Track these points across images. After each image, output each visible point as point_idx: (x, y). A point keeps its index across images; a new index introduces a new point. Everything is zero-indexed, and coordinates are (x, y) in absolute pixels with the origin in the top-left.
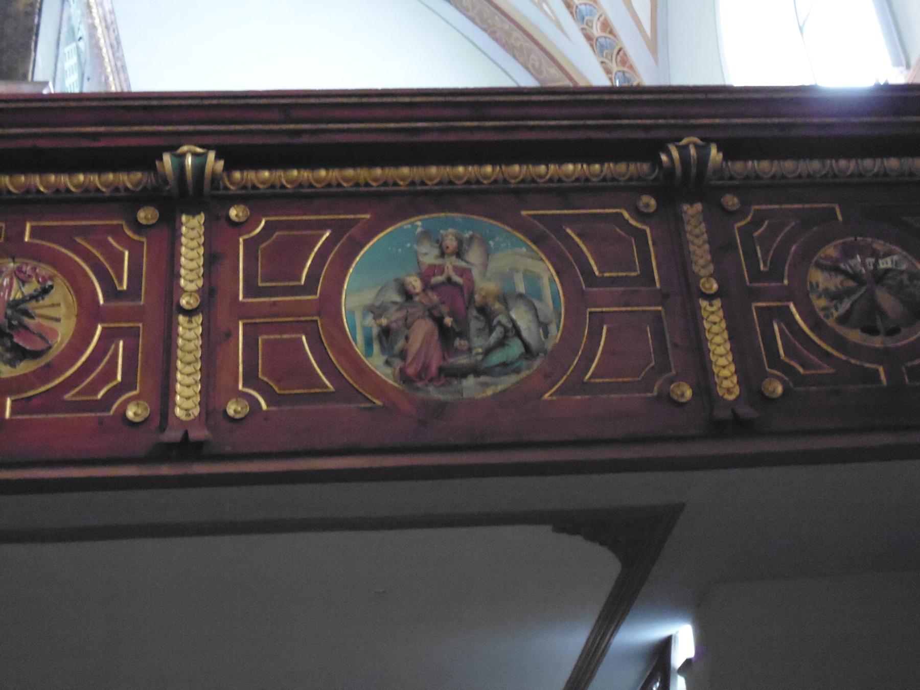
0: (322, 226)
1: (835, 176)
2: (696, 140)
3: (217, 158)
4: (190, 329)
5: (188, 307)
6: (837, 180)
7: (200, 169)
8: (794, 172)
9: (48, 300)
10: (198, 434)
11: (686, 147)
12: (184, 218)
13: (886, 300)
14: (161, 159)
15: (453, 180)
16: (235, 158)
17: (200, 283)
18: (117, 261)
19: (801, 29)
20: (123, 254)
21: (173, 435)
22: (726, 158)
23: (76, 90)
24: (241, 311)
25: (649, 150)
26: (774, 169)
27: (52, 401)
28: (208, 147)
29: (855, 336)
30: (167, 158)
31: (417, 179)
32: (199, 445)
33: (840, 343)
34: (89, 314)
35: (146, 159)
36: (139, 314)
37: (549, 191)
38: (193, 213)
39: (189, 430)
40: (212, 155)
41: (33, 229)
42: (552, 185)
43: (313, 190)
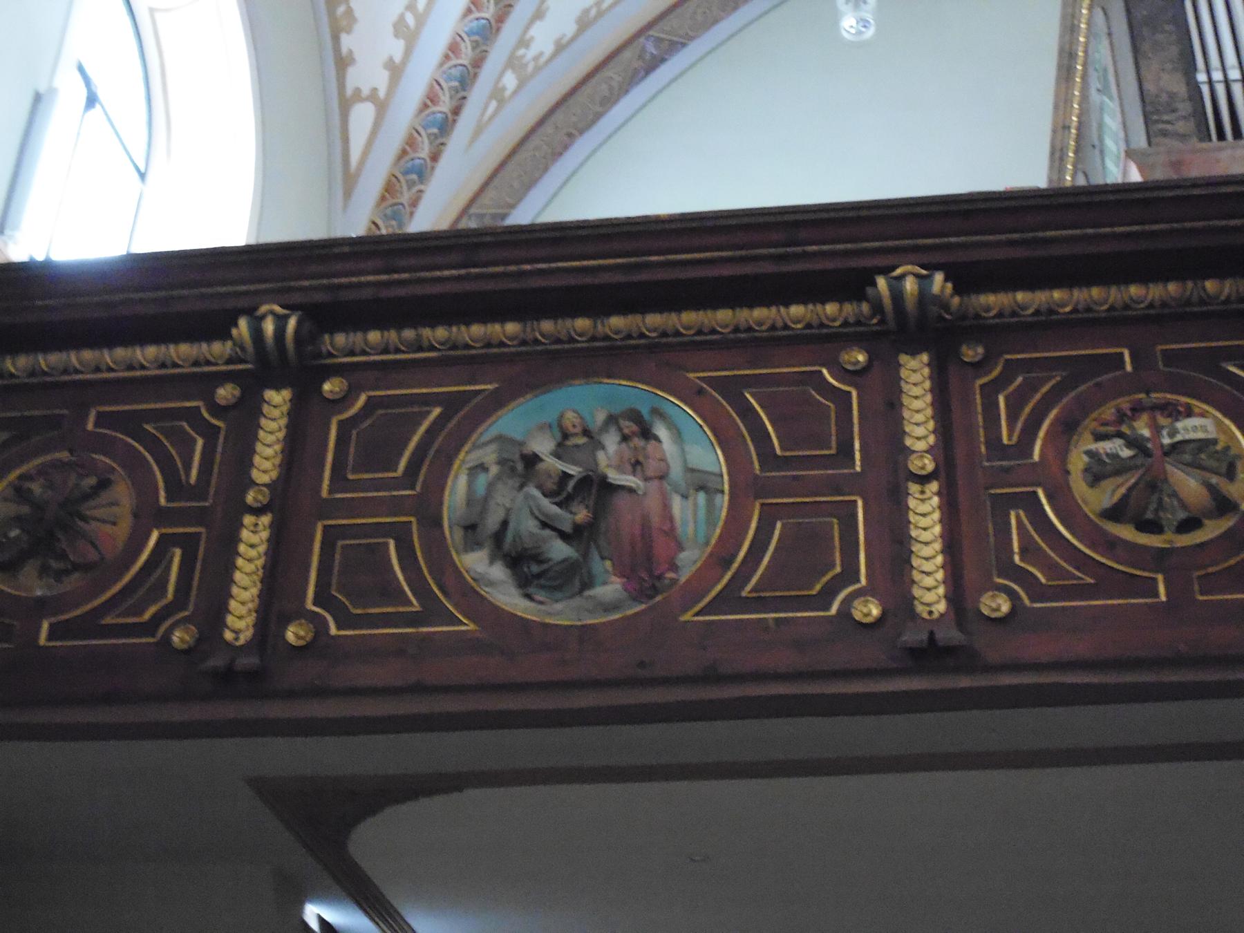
0: (428, 401)
1: (822, 325)
2: (277, 309)
3: (946, 280)
4: (923, 500)
5: (256, 505)
6: (1166, 311)
7: (924, 296)
8: (1105, 302)
9: (105, 497)
10: (950, 635)
11: (902, 277)
12: (925, 357)
13: (1189, 485)
14: (874, 284)
15: (1053, 307)
16: (967, 279)
17: (274, 474)
18: (186, 447)
19: (142, 176)
20: (194, 441)
21: (913, 637)
22: (957, 290)
23: (1120, 181)
24: (327, 508)
25: (853, 285)
26: (1226, 291)
27: (89, 626)
28: (932, 267)
29: (1126, 532)
30: (243, 323)
31: (743, 325)
32: (950, 650)
33: (1111, 545)
34: (147, 515)
35: (853, 285)
36: (201, 516)
37: (737, 344)
38: (914, 353)
39: (935, 629)
40: (939, 277)
41: (100, 415)
42: (1152, 312)
43: (790, 332)
